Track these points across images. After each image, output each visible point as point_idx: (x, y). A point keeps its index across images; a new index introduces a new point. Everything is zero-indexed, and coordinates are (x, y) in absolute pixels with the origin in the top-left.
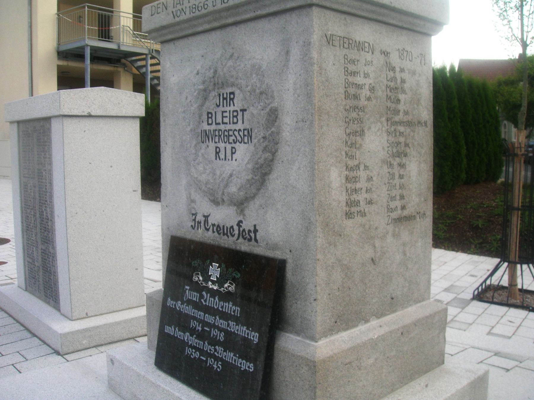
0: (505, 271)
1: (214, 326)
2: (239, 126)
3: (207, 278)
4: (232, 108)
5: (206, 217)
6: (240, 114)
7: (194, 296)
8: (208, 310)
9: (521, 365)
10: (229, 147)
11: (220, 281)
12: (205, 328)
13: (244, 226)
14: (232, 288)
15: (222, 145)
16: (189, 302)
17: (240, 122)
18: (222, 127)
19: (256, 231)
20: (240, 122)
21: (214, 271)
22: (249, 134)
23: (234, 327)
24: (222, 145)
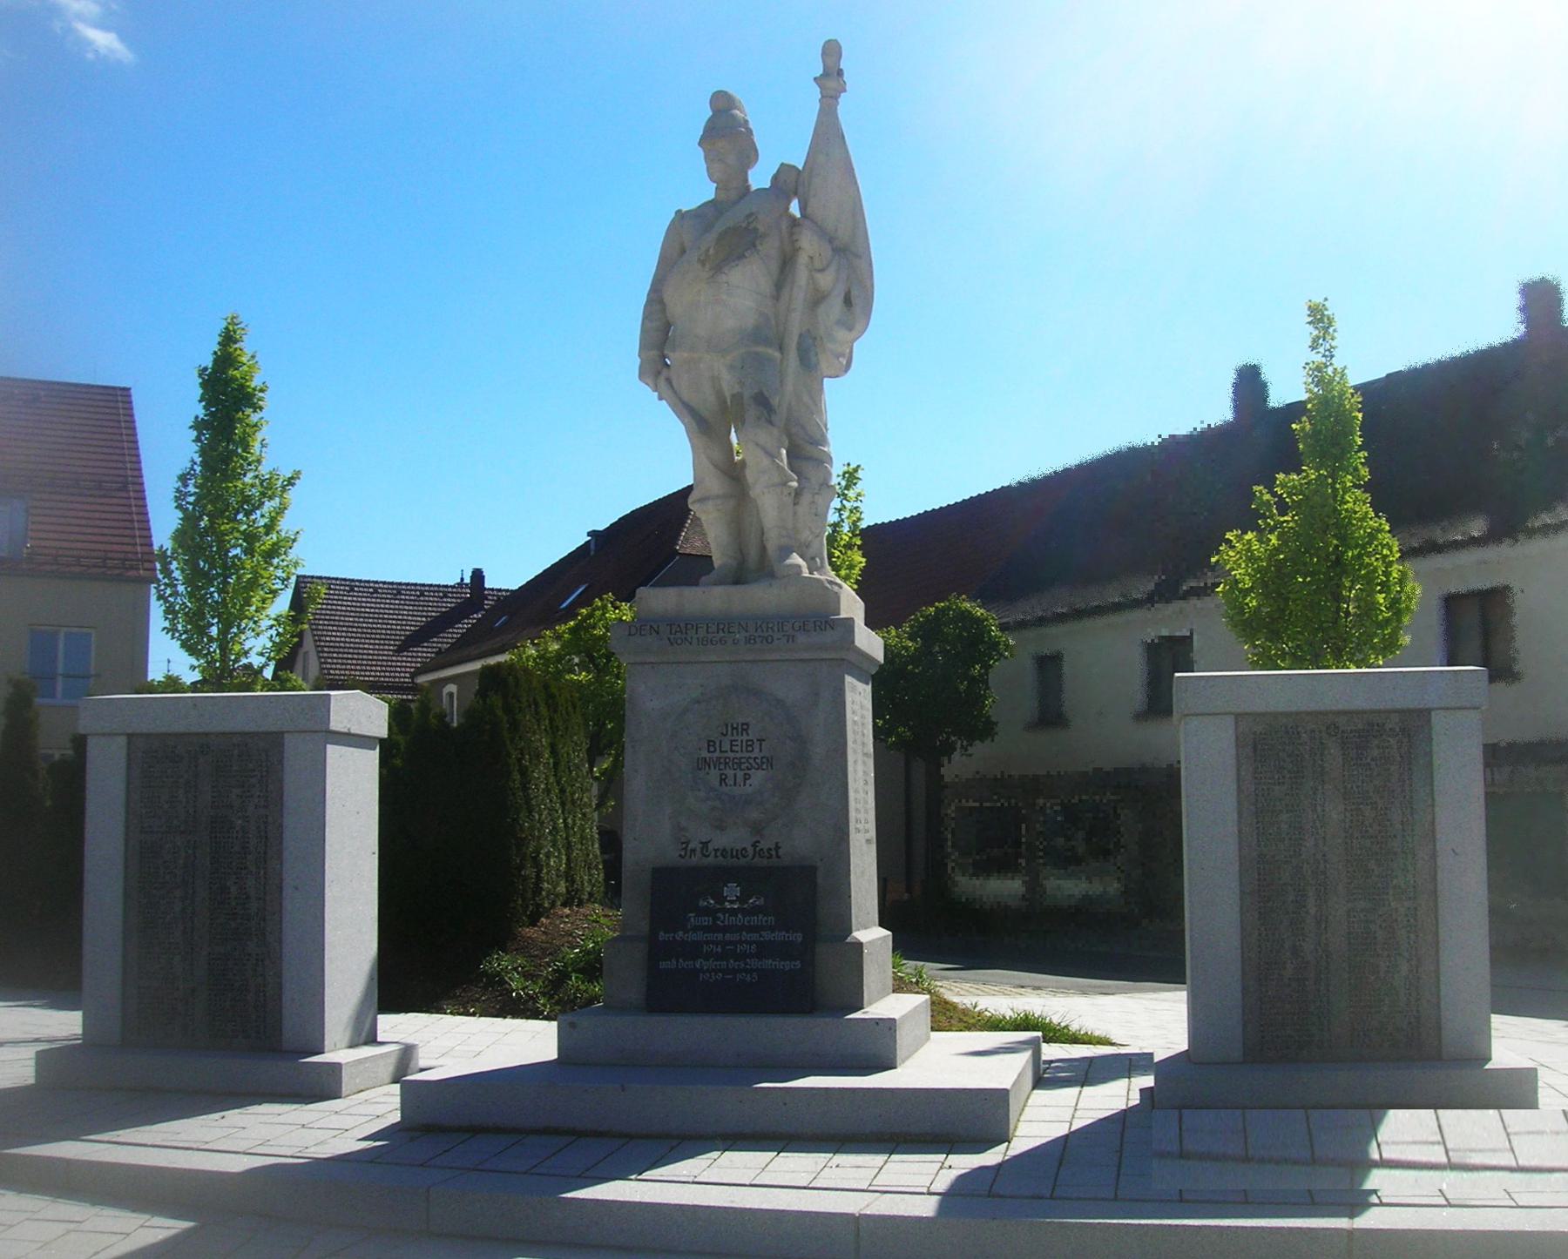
0: (37, 1040)
1: (741, 942)
2: (756, 753)
3: (721, 899)
4: (745, 737)
5: (705, 844)
6: (757, 745)
7: (706, 921)
8: (725, 930)
9: (82, 1227)
10: (740, 774)
11: (742, 899)
12: (663, 965)
13: (760, 846)
14: (761, 902)
15: (730, 773)
16: (695, 929)
17: (757, 750)
18: (732, 755)
19: (777, 847)
20: (757, 750)
21: (732, 891)
22: (769, 762)
23: (767, 936)
24: (730, 773)
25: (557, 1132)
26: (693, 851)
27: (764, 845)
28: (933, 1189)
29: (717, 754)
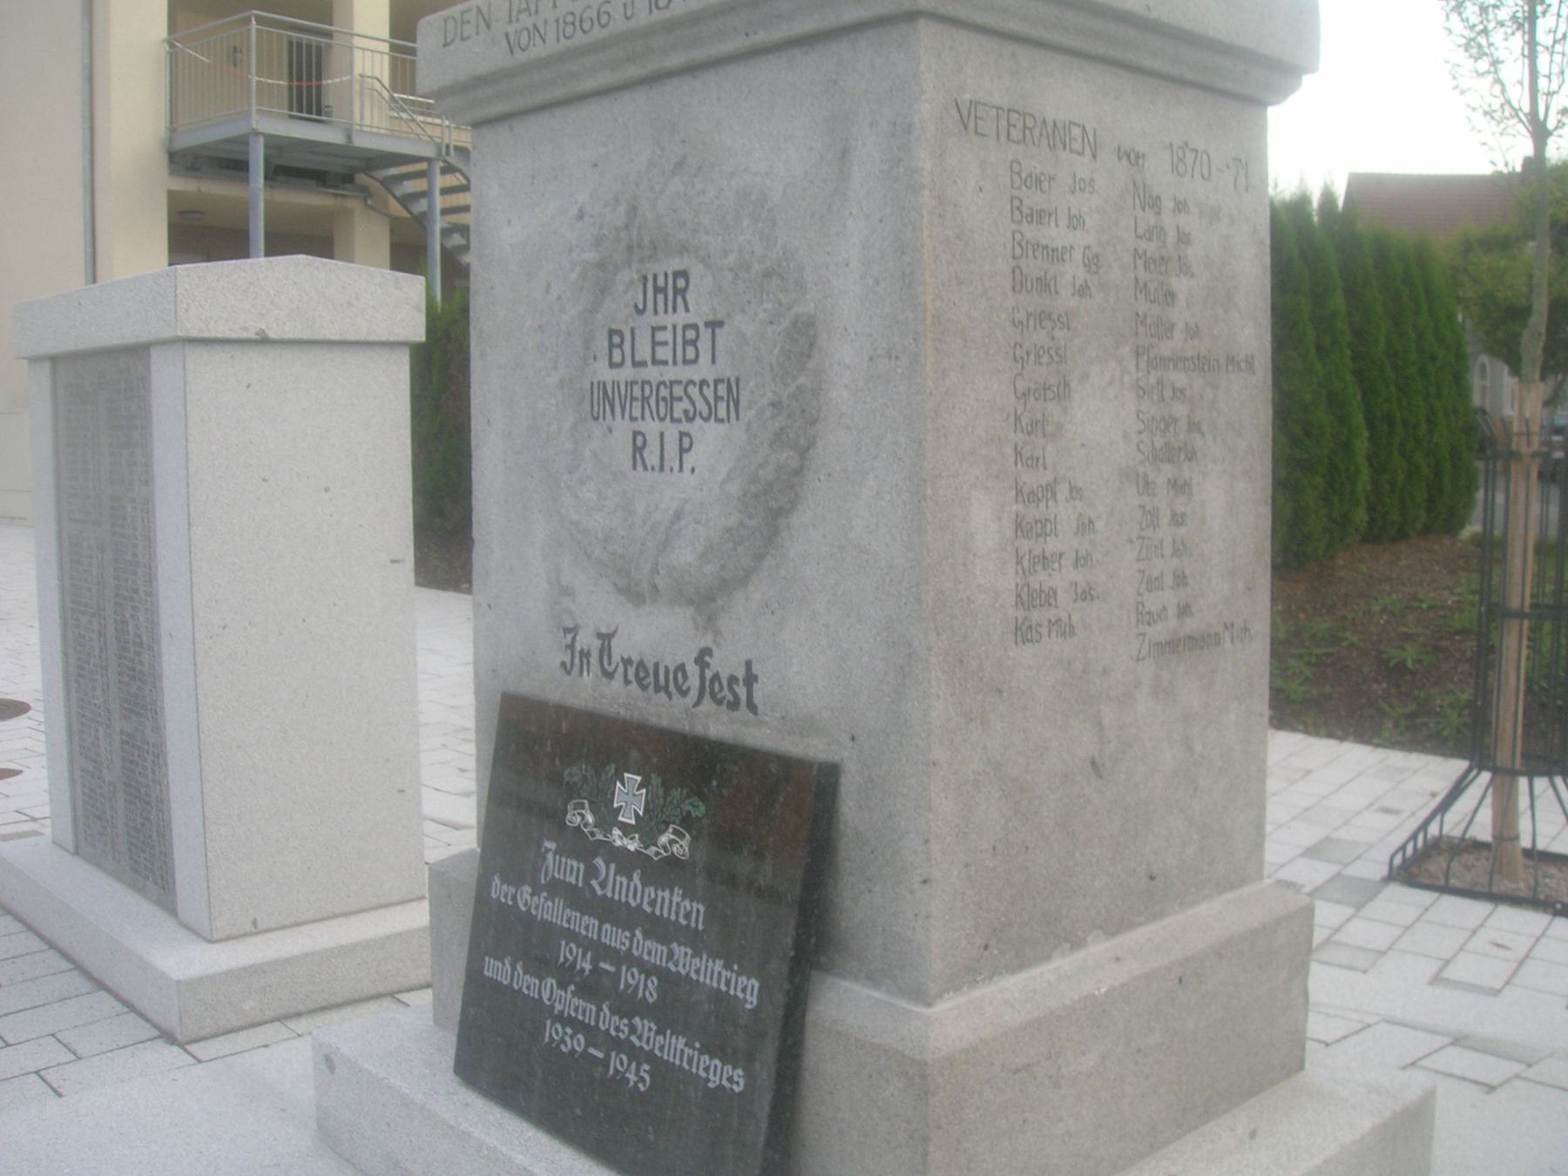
1: (628, 959)
3: (608, 817)
4: (681, 318)
5: (606, 638)
7: (571, 870)
8: (609, 911)
9: (1530, 1073)
10: (672, 432)
13: (717, 664)
14: (682, 848)
16: (555, 888)
17: (705, 358)
19: (751, 679)
20: (705, 358)
22: (730, 393)
23: (685, 961)
24: (651, 427)
25: (65, 956)
26: (585, 655)
27: (726, 663)
28: (192, 1061)
29: (627, 373)
